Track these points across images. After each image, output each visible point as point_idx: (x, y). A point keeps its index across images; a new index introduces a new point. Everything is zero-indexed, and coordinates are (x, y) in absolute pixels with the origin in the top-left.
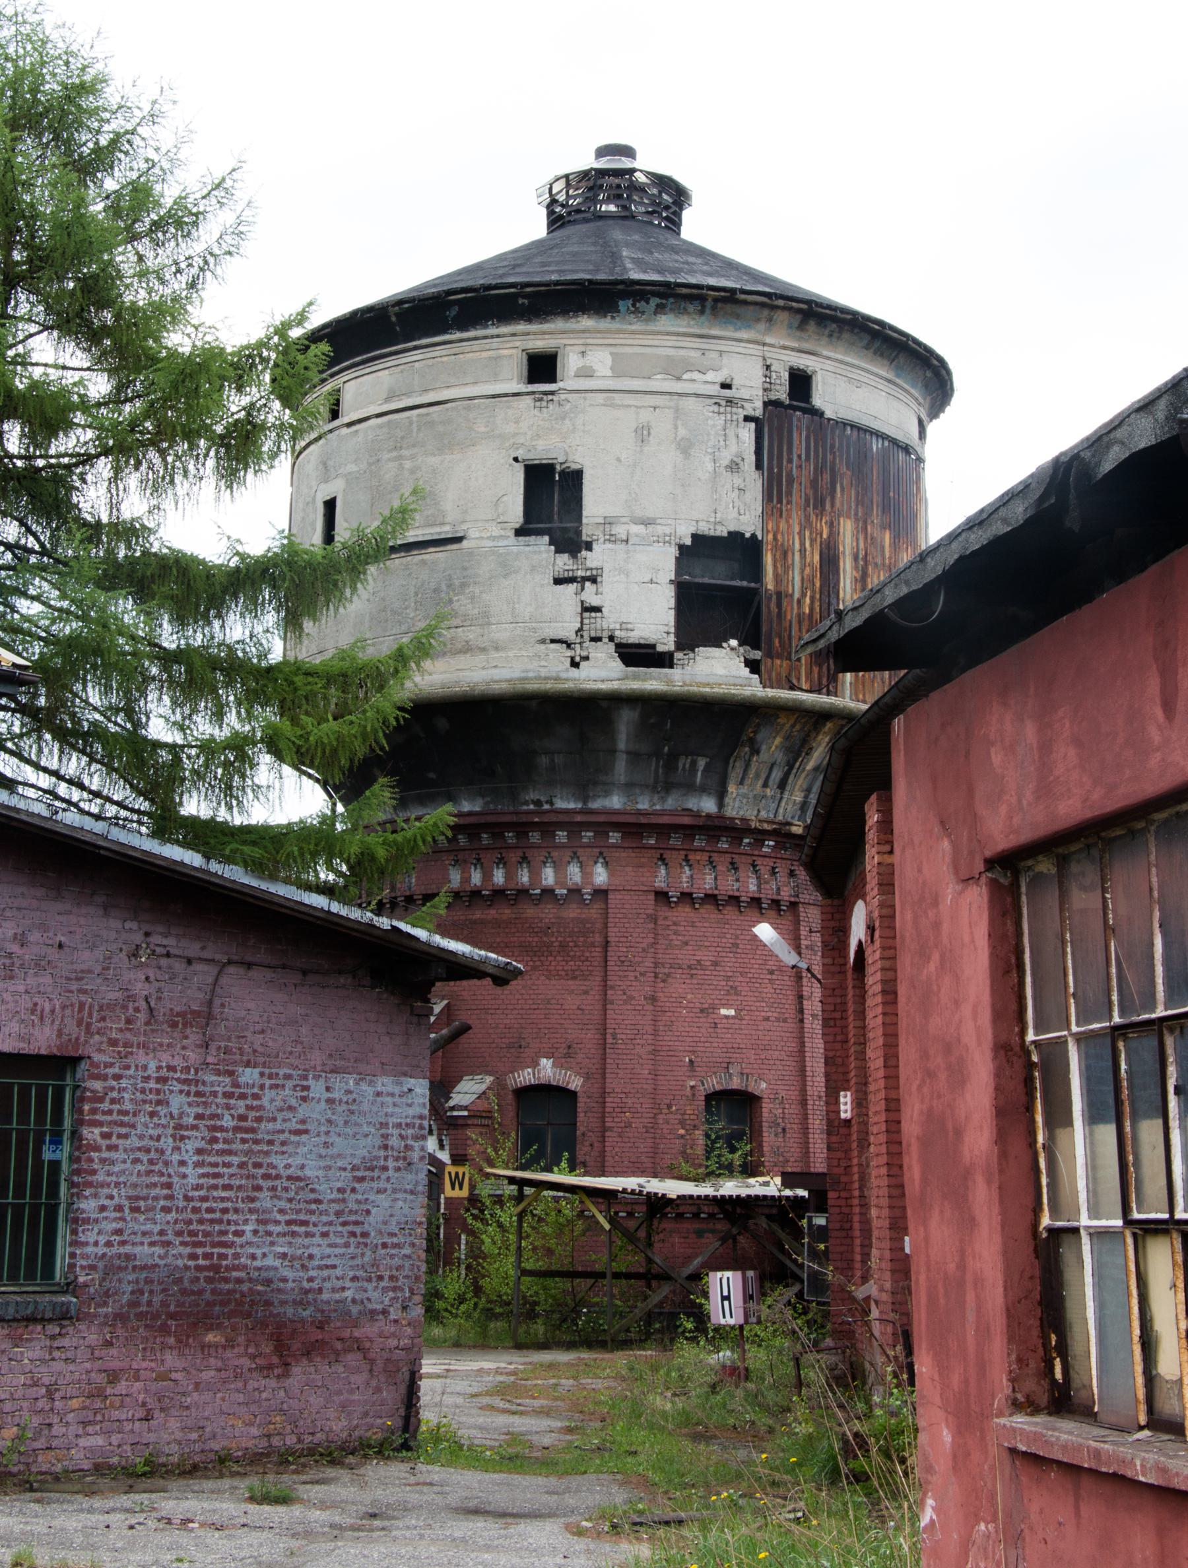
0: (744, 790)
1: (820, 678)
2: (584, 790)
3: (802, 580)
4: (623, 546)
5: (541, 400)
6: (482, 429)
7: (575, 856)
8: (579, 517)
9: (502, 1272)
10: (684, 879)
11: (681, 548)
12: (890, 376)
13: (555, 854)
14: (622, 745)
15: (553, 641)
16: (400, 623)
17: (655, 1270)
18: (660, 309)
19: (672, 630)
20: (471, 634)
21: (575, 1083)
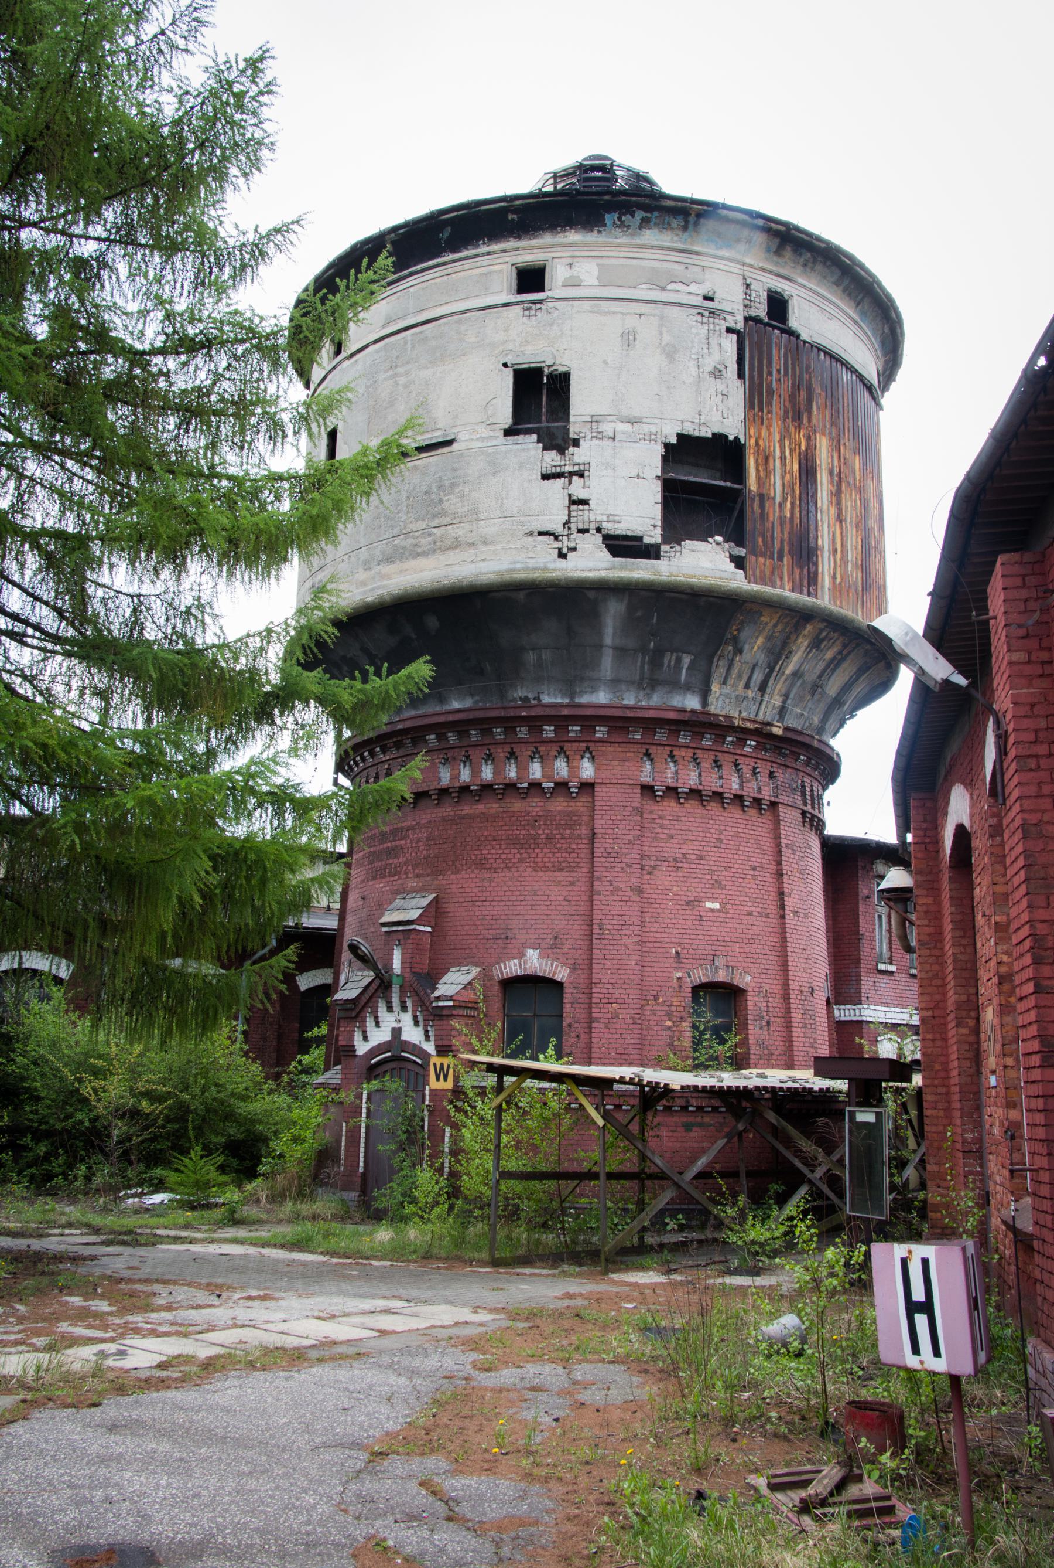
0: (727, 690)
1: (801, 580)
2: (570, 685)
3: (783, 485)
4: (610, 443)
5: (529, 309)
6: (473, 340)
7: (562, 751)
8: (568, 420)
9: (478, 1172)
10: (669, 775)
11: (667, 446)
12: (857, 318)
13: (542, 749)
14: (608, 640)
15: (540, 534)
16: (393, 527)
17: (650, 1169)
18: (645, 223)
19: (659, 523)
20: (460, 531)
21: (561, 974)
